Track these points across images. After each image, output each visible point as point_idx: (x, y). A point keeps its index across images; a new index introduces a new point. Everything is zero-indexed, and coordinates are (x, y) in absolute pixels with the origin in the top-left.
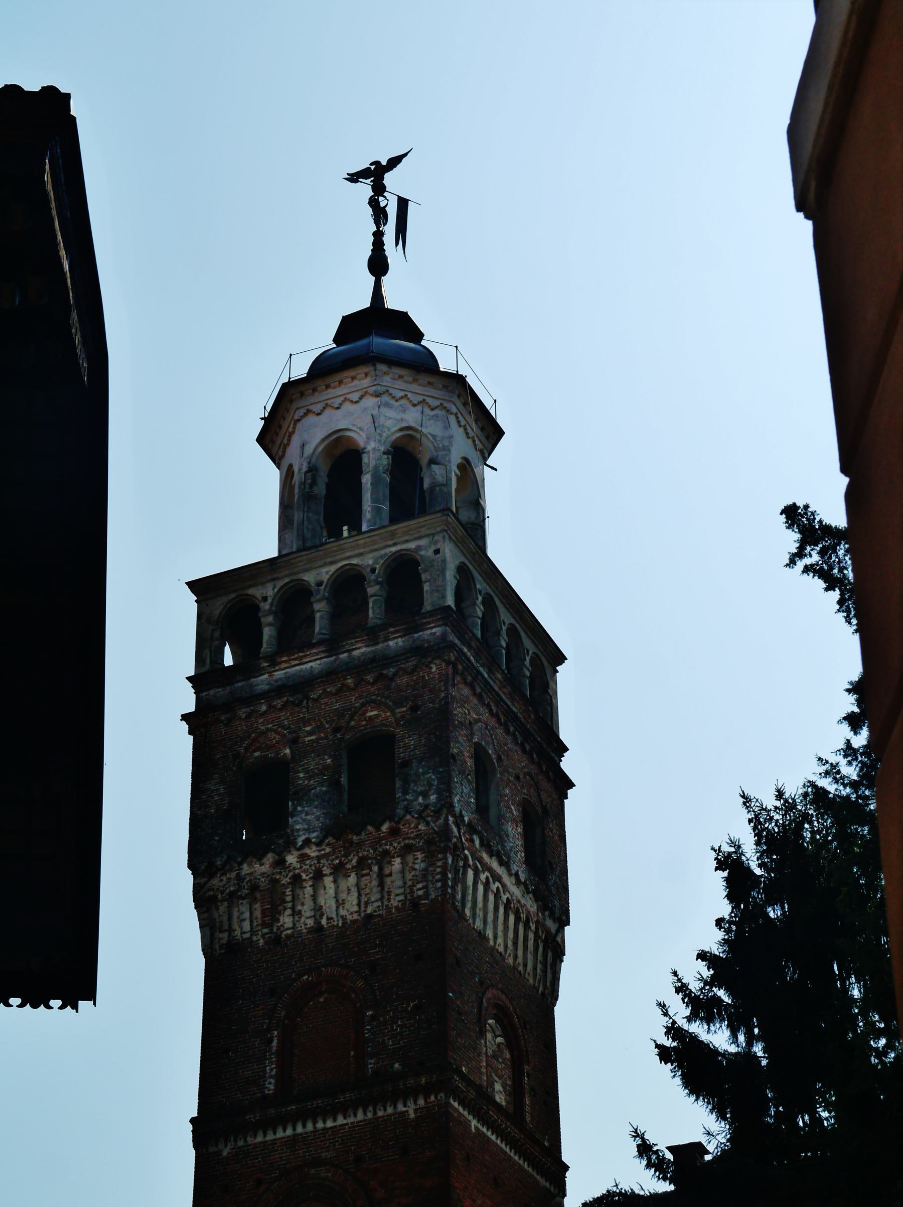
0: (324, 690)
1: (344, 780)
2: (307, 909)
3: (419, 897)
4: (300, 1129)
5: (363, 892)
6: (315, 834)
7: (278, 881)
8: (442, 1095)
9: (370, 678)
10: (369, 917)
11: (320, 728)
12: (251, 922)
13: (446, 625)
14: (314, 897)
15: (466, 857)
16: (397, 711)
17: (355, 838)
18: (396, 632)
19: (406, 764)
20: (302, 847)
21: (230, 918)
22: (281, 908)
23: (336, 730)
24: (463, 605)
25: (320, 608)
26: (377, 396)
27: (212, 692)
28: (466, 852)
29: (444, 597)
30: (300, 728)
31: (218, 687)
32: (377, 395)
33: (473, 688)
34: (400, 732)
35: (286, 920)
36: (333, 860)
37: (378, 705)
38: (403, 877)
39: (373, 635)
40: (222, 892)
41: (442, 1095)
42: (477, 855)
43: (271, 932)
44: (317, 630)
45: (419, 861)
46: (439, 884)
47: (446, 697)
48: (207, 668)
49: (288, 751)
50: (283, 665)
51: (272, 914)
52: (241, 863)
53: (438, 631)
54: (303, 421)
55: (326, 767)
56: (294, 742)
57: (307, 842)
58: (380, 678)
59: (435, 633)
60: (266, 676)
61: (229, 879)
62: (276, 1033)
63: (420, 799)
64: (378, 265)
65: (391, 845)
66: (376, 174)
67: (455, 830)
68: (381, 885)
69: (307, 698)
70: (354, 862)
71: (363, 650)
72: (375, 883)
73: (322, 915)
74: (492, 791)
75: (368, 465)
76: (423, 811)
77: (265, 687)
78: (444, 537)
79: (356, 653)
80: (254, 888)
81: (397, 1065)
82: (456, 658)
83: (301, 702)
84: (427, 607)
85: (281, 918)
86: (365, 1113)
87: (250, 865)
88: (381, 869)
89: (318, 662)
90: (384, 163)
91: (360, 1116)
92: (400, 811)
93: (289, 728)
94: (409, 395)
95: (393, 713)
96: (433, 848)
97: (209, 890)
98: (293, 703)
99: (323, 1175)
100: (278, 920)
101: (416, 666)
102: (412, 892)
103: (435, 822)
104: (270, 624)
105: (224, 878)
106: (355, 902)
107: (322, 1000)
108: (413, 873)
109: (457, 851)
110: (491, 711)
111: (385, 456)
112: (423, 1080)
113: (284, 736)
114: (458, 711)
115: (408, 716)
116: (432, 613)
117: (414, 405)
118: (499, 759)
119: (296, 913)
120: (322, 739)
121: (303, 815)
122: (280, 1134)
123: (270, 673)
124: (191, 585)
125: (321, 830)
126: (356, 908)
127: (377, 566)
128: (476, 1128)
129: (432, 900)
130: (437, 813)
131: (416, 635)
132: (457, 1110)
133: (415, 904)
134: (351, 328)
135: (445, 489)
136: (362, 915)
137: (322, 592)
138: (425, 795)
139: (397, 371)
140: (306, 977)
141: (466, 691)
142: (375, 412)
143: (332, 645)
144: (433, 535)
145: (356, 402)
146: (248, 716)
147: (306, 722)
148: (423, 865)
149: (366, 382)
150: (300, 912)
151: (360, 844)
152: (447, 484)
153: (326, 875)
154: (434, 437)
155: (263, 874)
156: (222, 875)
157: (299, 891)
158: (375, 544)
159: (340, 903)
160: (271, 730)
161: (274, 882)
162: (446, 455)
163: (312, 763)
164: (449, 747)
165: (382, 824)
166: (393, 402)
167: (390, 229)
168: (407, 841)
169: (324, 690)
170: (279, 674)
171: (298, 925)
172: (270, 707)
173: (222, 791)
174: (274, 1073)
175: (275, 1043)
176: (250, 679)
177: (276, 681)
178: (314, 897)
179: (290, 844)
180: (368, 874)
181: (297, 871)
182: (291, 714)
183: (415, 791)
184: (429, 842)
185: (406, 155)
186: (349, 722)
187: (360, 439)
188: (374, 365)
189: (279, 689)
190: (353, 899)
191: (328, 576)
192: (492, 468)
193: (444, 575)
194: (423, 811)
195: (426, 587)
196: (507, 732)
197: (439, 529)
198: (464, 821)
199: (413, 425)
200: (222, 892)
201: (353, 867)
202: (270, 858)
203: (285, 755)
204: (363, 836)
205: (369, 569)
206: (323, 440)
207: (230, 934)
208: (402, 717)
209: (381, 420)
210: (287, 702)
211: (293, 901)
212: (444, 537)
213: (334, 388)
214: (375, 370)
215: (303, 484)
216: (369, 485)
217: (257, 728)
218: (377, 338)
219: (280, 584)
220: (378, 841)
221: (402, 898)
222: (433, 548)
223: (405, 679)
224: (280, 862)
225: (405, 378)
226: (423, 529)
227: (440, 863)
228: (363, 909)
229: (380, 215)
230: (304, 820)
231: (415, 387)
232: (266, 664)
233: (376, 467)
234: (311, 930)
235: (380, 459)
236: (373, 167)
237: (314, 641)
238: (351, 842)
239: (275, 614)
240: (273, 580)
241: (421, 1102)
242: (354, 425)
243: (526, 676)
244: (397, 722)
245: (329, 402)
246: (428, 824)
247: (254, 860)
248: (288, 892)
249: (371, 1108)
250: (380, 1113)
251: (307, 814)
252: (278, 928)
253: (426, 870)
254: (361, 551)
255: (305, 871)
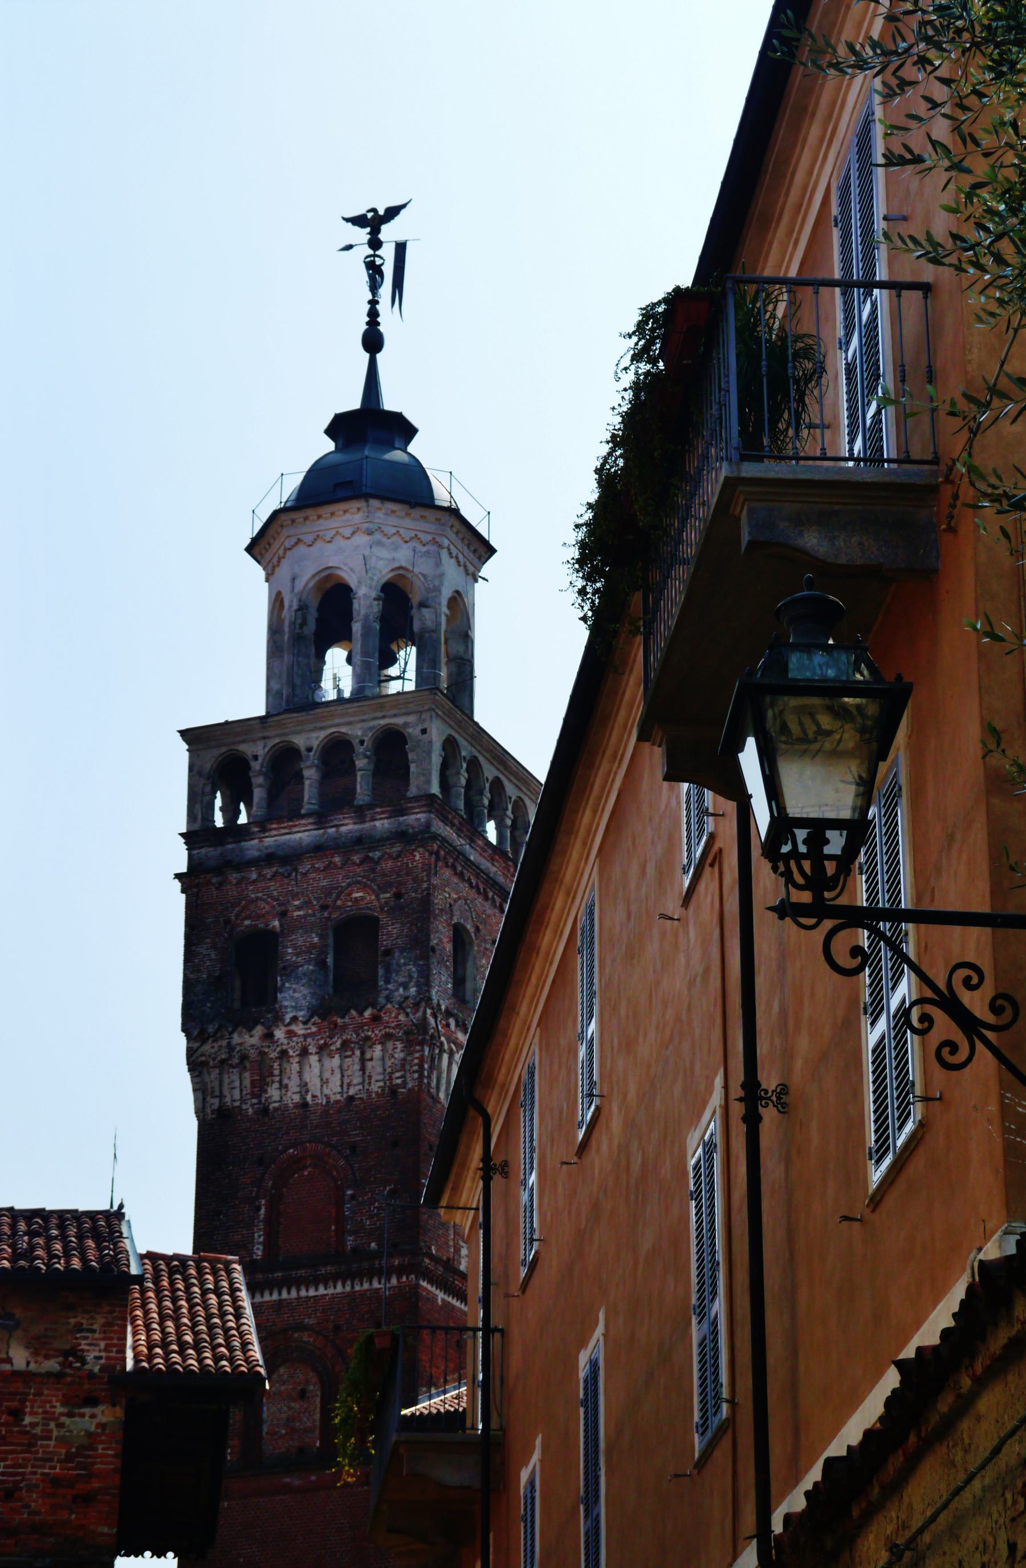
0: (313, 864)
1: (330, 960)
2: (293, 1084)
3: (397, 1085)
4: (285, 1295)
5: (346, 1074)
6: (301, 1013)
7: (265, 1053)
8: (413, 1276)
9: (356, 858)
10: (351, 1099)
11: (308, 903)
12: (241, 1090)
13: (430, 812)
14: (300, 1073)
15: (442, 1043)
16: (382, 896)
17: (339, 1020)
18: (382, 813)
19: (388, 952)
20: (289, 1024)
21: (221, 1085)
22: (269, 1079)
23: (324, 907)
24: (448, 773)
25: (311, 775)
26: (369, 534)
27: (203, 851)
28: (443, 1039)
29: (429, 782)
30: (289, 902)
31: (209, 846)
32: (370, 533)
33: (454, 867)
34: (384, 919)
35: (273, 1092)
36: (318, 1040)
37: (365, 887)
38: (384, 1065)
39: (361, 813)
40: (214, 1059)
41: (413, 1276)
42: (453, 1038)
43: (260, 1103)
44: (306, 798)
45: (398, 1050)
46: (416, 1075)
47: (428, 889)
48: (196, 827)
49: (276, 923)
50: (274, 833)
51: (260, 1086)
52: (231, 1033)
53: (422, 817)
54: (295, 550)
55: (313, 946)
56: (283, 914)
57: (294, 1019)
58: (366, 859)
59: (419, 819)
60: (256, 841)
61: (221, 1046)
62: (263, 1202)
63: (401, 990)
64: (373, 341)
65: (373, 1031)
66: (373, 222)
67: (432, 1021)
68: (363, 1069)
69: (296, 870)
70: (338, 1044)
71: (350, 827)
72: (357, 1067)
73: (307, 1091)
74: (469, 963)
75: (359, 615)
76: (403, 1002)
77: (256, 854)
78: (431, 717)
79: (343, 829)
80: (244, 1057)
81: (373, 1245)
82: (439, 847)
83: (290, 875)
84: (413, 791)
85: (269, 1089)
86: (344, 1286)
87: (240, 1035)
88: (363, 1053)
89: (307, 833)
90: (381, 212)
91: (339, 1288)
92: (382, 1000)
93: (277, 900)
94: (402, 531)
95: (377, 896)
96: (411, 1038)
97: (202, 1055)
98: (282, 874)
99: (305, 1339)
100: (266, 1091)
101: (401, 852)
102: (391, 1079)
103: (414, 1014)
104: (260, 786)
105: (215, 1045)
106: (338, 1083)
107: (306, 1173)
108: (393, 1060)
109: (433, 1041)
110: (471, 884)
111: (376, 603)
112: (397, 1262)
113: (273, 907)
114: (439, 899)
115: (392, 903)
116: (417, 799)
117: (406, 542)
118: (477, 930)
119: (283, 1087)
120: (310, 915)
121: (291, 992)
122: (267, 1297)
123: (261, 839)
124: (184, 734)
125: (308, 1009)
126: (339, 1089)
127: (366, 739)
128: (443, 1300)
129: (409, 1090)
130: (416, 1006)
131: (401, 819)
132: (426, 1289)
133: (393, 1091)
134: (341, 427)
135: (434, 635)
136: (345, 1095)
137: (312, 758)
138: (406, 987)
139: (390, 506)
140: (291, 1151)
141: (447, 873)
142: (367, 552)
143: (321, 818)
144: (421, 712)
145: (348, 538)
146: (239, 882)
147: (295, 896)
148: (402, 1055)
149: (358, 518)
150: (286, 1086)
151: (344, 1027)
152: (436, 630)
153: (311, 1054)
154: (424, 576)
155: (253, 1046)
156: (214, 1041)
157: (285, 1065)
158: (364, 714)
159: (324, 1082)
160: (261, 899)
161: (262, 1054)
162: (436, 596)
163: (300, 938)
164: (429, 940)
165: (365, 1009)
166: (384, 540)
167: (386, 290)
168: (387, 1030)
169: (313, 864)
170: (269, 841)
171: (284, 1098)
172: (260, 875)
173: (213, 956)
174: (261, 1240)
175: (262, 1211)
176: (240, 842)
177: (267, 848)
178: (300, 1073)
179: (278, 1019)
180: (350, 1056)
181: (284, 1047)
182: (281, 885)
183: (396, 982)
184: (407, 1033)
185: (404, 206)
186: (335, 901)
187: (352, 581)
188: (367, 501)
189: (270, 858)
190: (335, 1081)
191: (317, 743)
192: (484, 579)
193: (430, 758)
194: (403, 1002)
195: (413, 768)
196: (486, 898)
197: (426, 707)
198: (440, 1009)
199: (404, 564)
200: (214, 1059)
201: (337, 1049)
202: (259, 1030)
203: (274, 927)
204: (347, 1020)
205: (357, 741)
206: (314, 576)
207: (221, 1101)
208: (386, 903)
209: (372, 562)
210: (276, 873)
211: (280, 1075)
212: (431, 717)
213: (326, 519)
214: (368, 506)
215: (293, 624)
216: (359, 635)
217: (247, 896)
218: (370, 431)
219: (271, 743)
220: (361, 1026)
221: (381, 1084)
222: (420, 727)
223: (390, 864)
224: (269, 1036)
225: (398, 513)
226: (411, 705)
227: (417, 1055)
228: (345, 1090)
229: (374, 270)
230: (292, 997)
231: (407, 522)
232: (256, 829)
233: (367, 617)
234: (297, 1106)
235: (370, 606)
236: (370, 215)
237: (303, 811)
238: (336, 1025)
239: (265, 775)
240: (264, 738)
241: (394, 1281)
242: (345, 564)
243: (507, 827)
244: (382, 908)
245: (321, 533)
246: (407, 1015)
247: (244, 1030)
248: (276, 1065)
249: (349, 1282)
250: (357, 1288)
251: (295, 991)
252: (266, 1100)
253: (404, 1060)
254: (352, 719)
255: (293, 1048)
